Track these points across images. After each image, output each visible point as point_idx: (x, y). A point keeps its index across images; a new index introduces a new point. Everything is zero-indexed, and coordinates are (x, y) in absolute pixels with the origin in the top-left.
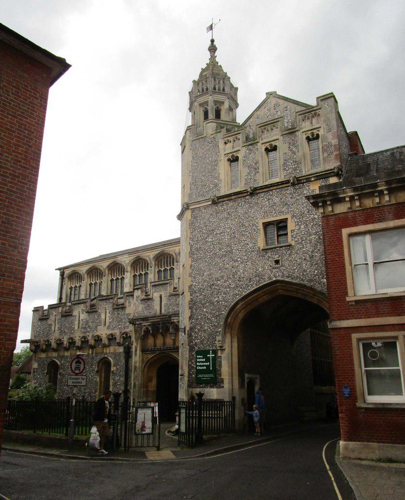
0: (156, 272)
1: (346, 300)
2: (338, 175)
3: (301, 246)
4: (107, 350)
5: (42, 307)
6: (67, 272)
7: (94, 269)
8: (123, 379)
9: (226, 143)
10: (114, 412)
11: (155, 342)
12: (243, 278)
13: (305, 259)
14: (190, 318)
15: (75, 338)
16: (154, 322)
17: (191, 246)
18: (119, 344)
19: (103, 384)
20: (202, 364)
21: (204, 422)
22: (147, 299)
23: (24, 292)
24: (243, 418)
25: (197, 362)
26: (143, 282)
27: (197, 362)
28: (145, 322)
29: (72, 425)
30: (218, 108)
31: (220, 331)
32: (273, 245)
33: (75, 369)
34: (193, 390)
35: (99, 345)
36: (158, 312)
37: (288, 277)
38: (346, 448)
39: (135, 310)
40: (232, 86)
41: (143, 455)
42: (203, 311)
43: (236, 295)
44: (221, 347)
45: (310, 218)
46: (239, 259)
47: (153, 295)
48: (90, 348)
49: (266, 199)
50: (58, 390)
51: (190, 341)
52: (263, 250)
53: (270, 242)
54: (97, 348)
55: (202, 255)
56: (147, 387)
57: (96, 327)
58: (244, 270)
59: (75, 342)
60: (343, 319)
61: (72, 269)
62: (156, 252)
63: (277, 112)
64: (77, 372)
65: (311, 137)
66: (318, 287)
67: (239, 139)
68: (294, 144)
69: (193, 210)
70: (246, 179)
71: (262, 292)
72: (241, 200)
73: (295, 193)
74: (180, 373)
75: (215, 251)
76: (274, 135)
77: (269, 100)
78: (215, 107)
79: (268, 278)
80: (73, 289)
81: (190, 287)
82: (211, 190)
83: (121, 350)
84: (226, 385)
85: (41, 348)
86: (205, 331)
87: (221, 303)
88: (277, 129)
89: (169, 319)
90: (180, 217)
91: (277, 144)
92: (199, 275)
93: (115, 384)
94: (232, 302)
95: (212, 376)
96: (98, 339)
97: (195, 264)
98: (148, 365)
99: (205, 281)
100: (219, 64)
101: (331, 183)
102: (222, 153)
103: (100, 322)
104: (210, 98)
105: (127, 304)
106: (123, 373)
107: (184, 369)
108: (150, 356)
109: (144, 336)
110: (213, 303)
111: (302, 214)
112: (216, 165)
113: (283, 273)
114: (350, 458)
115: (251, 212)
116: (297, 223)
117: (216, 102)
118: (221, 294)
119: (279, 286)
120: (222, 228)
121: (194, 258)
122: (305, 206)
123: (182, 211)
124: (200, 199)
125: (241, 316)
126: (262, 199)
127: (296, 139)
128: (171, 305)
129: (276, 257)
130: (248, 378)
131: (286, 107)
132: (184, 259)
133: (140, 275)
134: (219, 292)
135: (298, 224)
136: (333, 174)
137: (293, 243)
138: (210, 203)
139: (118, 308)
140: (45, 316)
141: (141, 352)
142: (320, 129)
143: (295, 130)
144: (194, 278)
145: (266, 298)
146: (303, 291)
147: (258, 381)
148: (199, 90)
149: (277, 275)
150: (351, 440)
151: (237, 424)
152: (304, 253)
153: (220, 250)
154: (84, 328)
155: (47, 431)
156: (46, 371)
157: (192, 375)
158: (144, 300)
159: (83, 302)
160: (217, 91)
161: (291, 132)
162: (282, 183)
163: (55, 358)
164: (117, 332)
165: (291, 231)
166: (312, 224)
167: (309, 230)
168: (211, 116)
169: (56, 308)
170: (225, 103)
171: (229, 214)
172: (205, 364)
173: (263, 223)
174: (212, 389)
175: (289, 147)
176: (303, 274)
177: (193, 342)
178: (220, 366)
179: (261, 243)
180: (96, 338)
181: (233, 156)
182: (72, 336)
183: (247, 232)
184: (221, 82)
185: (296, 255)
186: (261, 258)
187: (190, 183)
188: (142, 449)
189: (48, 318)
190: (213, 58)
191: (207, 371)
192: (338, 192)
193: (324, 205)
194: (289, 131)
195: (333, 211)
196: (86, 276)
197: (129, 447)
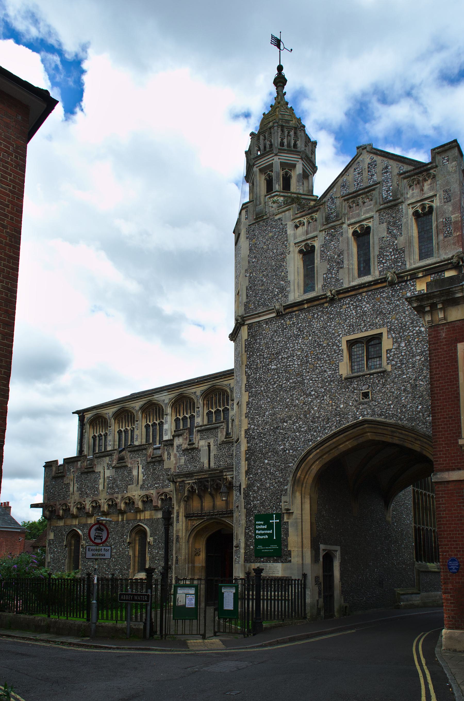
0: (205, 414)
1: (458, 442)
2: (456, 267)
3: (400, 372)
4: (142, 516)
5: (56, 461)
6: (88, 416)
7: (123, 410)
8: (162, 552)
9: (297, 227)
10: (147, 592)
11: (202, 506)
12: (319, 417)
13: (405, 390)
14: (247, 473)
15: (100, 501)
16: (201, 478)
17: (248, 377)
18: (156, 509)
19: (137, 559)
20: (263, 532)
21: (264, 605)
22: (191, 450)
23: (6, 431)
24: (318, 601)
25: (256, 529)
26: (189, 426)
27: (256, 529)
28: (189, 479)
29: (94, 609)
30: (286, 173)
31: (287, 489)
32: (360, 371)
33: (95, 538)
34: (250, 565)
35: (130, 509)
36: (206, 465)
37: (381, 415)
38: (450, 638)
39: (176, 464)
40: (307, 139)
41: (184, 644)
42: (264, 463)
43: (309, 440)
44: (288, 510)
45: (414, 332)
46: (313, 393)
47: (198, 443)
48: (118, 514)
49: (352, 307)
50: (80, 567)
51: (247, 503)
52: (346, 379)
53: (356, 367)
54: (129, 514)
55: (262, 389)
56: (193, 562)
57: (126, 488)
58: (320, 407)
59: (100, 506)
60: (453, 470)
61: (95, 412)
62: (204, 387)
63: (372, 175)
64: (97, 541)
65: (420, 211)
66: (423, 428)
67: (316, 220)
68: (395, 223)
69: (250, 326)
70: (325, 279)
71: (344, 437)
72: (317, 309)
73: (393, 296)
74: (235, 544)
75: (280, 382)
76: (367, 213)
77: (360, 158)
78: (282, 173)
79: (352, 417)
80: (97, 438)
81: (247, 431)
82: (275, 296)
83: (160, 515)
84: (295, 559)
85: (57, 514)
86: (266, 489)
87: (287, 452)
88: (372, 202)
89: (221, 474)
90: (233, 336)
91: (370, 224)
92: (259, 415)
93: (153, 559)
94: (303, 450)
95: (275, 547)
96: (130, 502)
97: (253, 400)
98: (196, 534)
99: (266, 424)
100: (289, 106)
101: (446, 276)
102: (292, 241)
103: (131, 480)
104: (276, 158)
105: (165, 456)
106: (162, 545)
107: (240, 539)
108: (196, 523)
109: (188, 497)
110: (277, 453)
111: (403, 328)
112: (283, 260)
113: (373, 411)
114: (455, 651)
115: (330, 326)
116: (395, 340)
117: (283, 165)
118: (288, 440)
119: (368, 427)
120: (290, 349)
121: (251, 393)
122: (406, 312)
123: (236, 326)
124: (260, 310)
125: (315, 468)
126: (347, 307)
127: (399, 215)
128: (222, 456)
129: (363, 388)
130: (323, 550)
131: (387, 167)
132: (241, 396)
133: (185, 419)
134: (285, 438)
135: (396, 342)
136: (450, 266)
137: (389, 368)
138: (274, 315)
139: (154, 462)
140: (61, 473)
141: (184, 518)
142: (434, 199)
143: (397, 202)
144: (253, 419)
145: (349, 445)
146: (401, 434)
147: (338, 554)
148: (259, 147)
149: (365, 413)
150: (457, 628)
151: (308, 609)
152: (404, 381)
153: (287, 380)
154: (112, 488)
155: (64, 614)
156: (65, 543)
157: (249, 546)
158: (187, 450)
159: (109, 454)
160: (285, 148)
161: (392, 206)
162: (376, 282)
163: (75, 526)
164: (153, 492)
165: (387, 350)
166: (416, 340)
167: (412, 348)
168: (277, 187)
169: (73, 462)
170: (297, 166)
171: (299, 330)
172: (266, 532)
173: (347, 341)
174: (275, 564)
175: (388, 229)
176: (402, 411)
177: (250, 504)
178: (287, 534)
179: (344, 370)
180: (127, 501)
181: (306, 245)
182: (95, 498)
183: (325, 354)
184: (292, 133)
185: (392, 384)
186: (344, 390)
187: (247, 287)
188: (183, 638)
189: (64, 476)
190: (280, 94)
191: (269, 541)
192: (454, 289)
193: (433, 307)
194: (389, 204)
195: (445, 318)
196: (113, 421)
197: (166, 635)
